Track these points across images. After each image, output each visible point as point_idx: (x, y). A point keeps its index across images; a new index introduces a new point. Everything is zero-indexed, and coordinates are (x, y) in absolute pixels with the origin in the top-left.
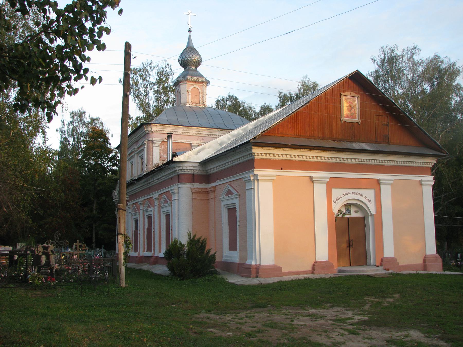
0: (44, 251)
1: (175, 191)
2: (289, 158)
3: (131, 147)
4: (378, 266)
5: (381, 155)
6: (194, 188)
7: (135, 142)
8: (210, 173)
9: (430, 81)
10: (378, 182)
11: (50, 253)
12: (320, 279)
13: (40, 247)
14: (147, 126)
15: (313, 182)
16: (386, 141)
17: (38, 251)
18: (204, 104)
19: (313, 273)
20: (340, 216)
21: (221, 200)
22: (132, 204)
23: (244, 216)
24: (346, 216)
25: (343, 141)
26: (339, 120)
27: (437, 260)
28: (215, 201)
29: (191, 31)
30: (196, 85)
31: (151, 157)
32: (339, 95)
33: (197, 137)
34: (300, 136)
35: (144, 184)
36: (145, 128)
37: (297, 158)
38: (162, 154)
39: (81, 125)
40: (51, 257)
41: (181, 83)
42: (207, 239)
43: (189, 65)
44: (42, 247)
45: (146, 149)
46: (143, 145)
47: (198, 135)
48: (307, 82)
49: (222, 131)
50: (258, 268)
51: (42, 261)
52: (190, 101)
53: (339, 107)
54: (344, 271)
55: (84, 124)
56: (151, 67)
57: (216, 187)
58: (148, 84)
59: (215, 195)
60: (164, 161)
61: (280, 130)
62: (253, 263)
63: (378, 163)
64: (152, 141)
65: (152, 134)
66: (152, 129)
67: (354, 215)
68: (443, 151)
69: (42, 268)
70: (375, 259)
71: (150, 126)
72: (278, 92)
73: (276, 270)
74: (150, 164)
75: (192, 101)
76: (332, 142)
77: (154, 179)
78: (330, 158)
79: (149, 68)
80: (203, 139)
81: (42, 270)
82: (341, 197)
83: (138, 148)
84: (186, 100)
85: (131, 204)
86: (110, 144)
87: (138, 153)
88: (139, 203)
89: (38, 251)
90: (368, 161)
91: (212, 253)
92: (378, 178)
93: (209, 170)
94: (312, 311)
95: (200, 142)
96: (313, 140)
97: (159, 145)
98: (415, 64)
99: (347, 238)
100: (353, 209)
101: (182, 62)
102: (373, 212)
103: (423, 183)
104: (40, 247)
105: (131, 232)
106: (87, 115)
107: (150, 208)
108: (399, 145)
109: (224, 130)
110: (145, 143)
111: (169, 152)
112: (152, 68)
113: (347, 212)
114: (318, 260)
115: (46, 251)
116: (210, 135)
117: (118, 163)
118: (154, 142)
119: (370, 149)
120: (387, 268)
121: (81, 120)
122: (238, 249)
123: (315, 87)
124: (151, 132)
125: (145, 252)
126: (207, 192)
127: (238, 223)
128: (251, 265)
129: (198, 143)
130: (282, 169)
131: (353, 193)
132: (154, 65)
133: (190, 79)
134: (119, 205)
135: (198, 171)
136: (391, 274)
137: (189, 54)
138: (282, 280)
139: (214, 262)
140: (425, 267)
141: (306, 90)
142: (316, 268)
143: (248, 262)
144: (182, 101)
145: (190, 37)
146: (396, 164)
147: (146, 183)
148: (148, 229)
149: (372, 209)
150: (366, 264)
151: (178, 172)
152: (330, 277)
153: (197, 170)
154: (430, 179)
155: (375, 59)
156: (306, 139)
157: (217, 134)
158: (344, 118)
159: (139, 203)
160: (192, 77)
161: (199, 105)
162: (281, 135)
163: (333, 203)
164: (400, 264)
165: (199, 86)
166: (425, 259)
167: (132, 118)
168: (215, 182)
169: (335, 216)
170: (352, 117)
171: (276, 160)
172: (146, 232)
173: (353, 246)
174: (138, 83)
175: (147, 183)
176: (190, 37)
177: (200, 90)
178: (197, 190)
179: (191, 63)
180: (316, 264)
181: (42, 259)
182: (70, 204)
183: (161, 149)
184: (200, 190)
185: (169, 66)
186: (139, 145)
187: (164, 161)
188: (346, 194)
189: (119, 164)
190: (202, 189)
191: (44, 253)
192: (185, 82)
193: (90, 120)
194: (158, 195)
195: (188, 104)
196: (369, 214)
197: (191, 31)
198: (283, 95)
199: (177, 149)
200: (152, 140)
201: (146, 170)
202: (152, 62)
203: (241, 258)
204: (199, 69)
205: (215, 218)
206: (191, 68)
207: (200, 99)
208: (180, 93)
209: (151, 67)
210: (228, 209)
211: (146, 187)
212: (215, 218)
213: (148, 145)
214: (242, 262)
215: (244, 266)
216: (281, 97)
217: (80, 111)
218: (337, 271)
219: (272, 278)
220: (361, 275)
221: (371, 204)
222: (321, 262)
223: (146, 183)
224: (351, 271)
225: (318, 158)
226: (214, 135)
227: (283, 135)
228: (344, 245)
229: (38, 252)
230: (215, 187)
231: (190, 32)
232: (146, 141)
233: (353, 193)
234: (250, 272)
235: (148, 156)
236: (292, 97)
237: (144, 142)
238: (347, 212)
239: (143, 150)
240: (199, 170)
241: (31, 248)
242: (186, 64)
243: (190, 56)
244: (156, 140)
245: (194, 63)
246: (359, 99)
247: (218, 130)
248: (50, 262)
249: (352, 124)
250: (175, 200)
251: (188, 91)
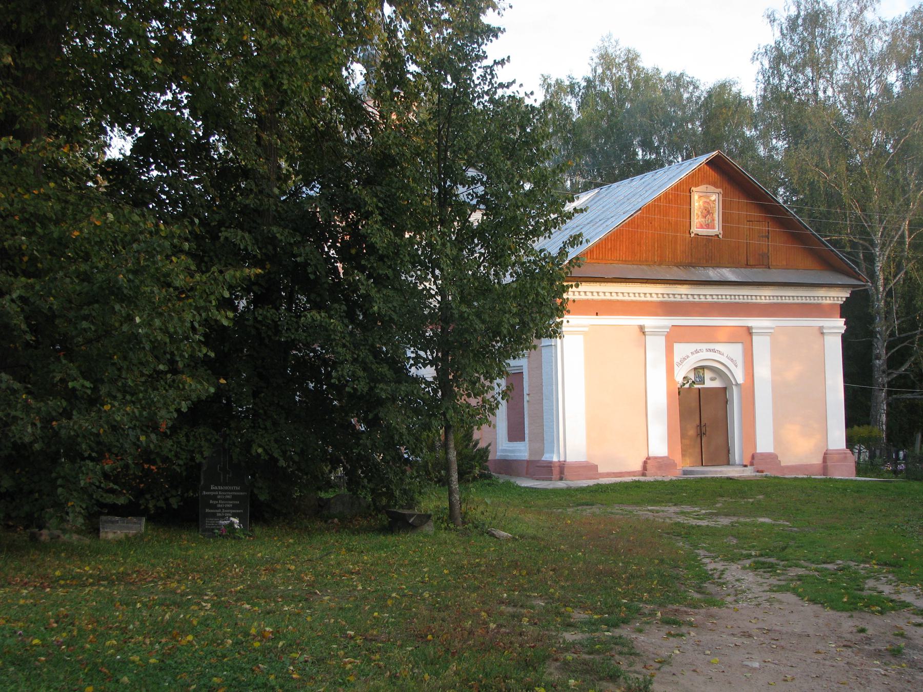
2: (608, 297)
4: (745, 466)
5: (755, 287)
9: (903, 63)
10: (749, 331)
12: (656, 481)
15: (644, 333)
16: (763, 262)
19: (644, 475)
20: (687, 386)
23: (538, 388)
24: (696, 386)
25: (693, 267)
26: (687, 232)
27: (845, 458)
32: (688, 191)
34: (626, 261)
37: (620, 297)
41: (576, 293)
48: (610, 51)
50: (562, 466)
53: (688, 212)
54: (691, 472)
61: (595, 252)
62: (555, 459)
63: (749, 301)
67: (709, 384)
68: (860, 277)
70: (741, 456)
73: (589, 468)
76: (675, 268)
78: (671, 296)
82: (688, 357)
90: (733, 297)
91: (482, 445)
92: (750, 325)
94: (650, 508)
96: (645, 267)
98: (870, 31)
99: (698, 422)
100: (708, 375)
102: (740, 380)
103: (825, 331)
108: (786, 268)
113: (698, 380)
114: (651, 455)
119: (736, 280)
120: (760, 469)
122: (527, 439)
123: (633, 60)
127: (526, 398)
128: (551, 462)
130: (597, 314)
131: (707, 350)
136: (766, 476)
138: (600, 483)
139: (487, 461)
140: (825, 467)
141: (609, 69)
142: (648, 466)
143: (546, 457)
146: (780, 301)
149: (739, 376)
150: (728, 464)
152: (671, 480)
154: (839, 324)
155: (777, 16)
156: (635, 267)
158: (695, 229)
162: (596, 261)
163: (675, 366)
164: (783, 464)
166: (826, 456)
169: (679, 386)
170: (708, 226)
171: (587, 301)
173: (707, 433)
180: (648, 461)
188: (697, 352)
196: (734, 383)
198: (553, 82)
203: (531, 452)
214: (533, 458)
215: (538, 464)
216: (549, 85)
218: (681, 472)
219: (584, 481)
220: (717, 478)
221: (736, 366)
222: (655, 458)
224: (702, 472)
225: (653, 295)
227: (599, 261)
228: (692, 432)
233: (707, 350)
234: (551, 472)
236: (576, 86)
238: (698, 380)
246: (721, 196)
249: (708, 238)
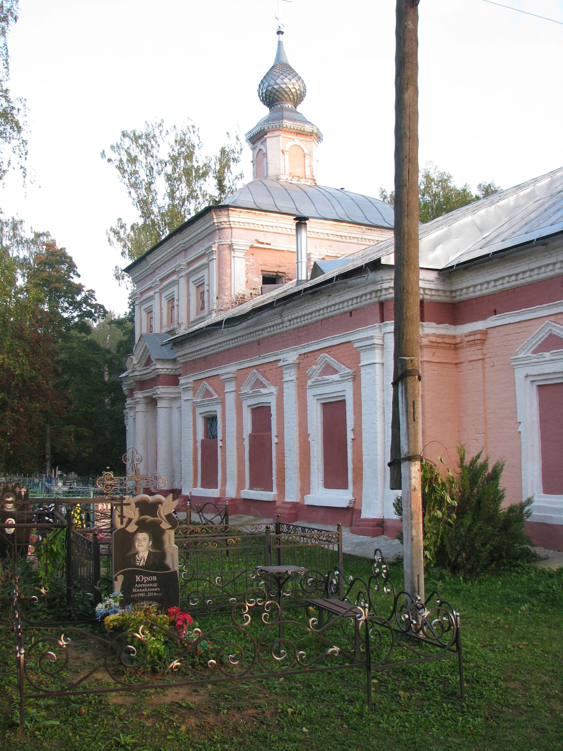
0: (145, 520)
1: (376, 341)
3: (169, 263)
6: (427, 335)
7: (180, 252)
8: (464, 297)
11: (165, 525)
13: (129, 504)
14: (219, 213)
17: (122, 517)
18: (314, 180)
21: (513, 364)
22: (194, 381)
28: (484, 368)
29: (282, 33)
30: (297, 140)
31: (227, 279)
33: (319, 241)
35: (244, 332)
36: (214, 217)
38: (250, 275)
39: (16, 245)
40: (166, 537)
41: (269, 135)
42: (504, 465)
43: (281, 99)
44: (138, 504)
45: (214, 265)
46: (207, 254)
47: (321, 236)
49: (370, 231)
51: (137, 553)
52: (287, 172)
55: (21, 242)
56: (161, 132)
57: (489, 331)
58: (156, 163)
59: (485, 351)
60: (254, 289)
64: (231, 246)
65: (230, 230)
66: (231, 219)
69: (138, 578)
71: (226, 213)
72: (379, 189)
74: (226, 296)
75: (292, 171)
77: (286, 319)
79: (157, 133)
80: (331, 246)
81: (139, 583)
83: (189, 264)
84: (280, 169)
85: (191, 380)
86: (79, 276)
87: (188, 276)
88: (222, 378)
89: (122, 517)
93: (455, 291)
95: (326, 251)
97: (244, 254)
101: (268, 93)
104: (129, 504)
105: (192, 442)
106: (25, 226)
107: (264, 386)
109: (372, 228)
110: (213, 249)
111: (300, 260)
112: (164, 133)
115: (149, 518)
116: (346, 237)
117: (93, 311)
118: (235, 247)
121: (15, 236)
123: (446, 180)
124: (226, 226)
125: (246, 490)
126: (452, 346)
129: (322, 253)
130: (495, 313)
132: (167, 126)
133: (289, 127)
134: (412, 361)
135: (433, 293)
137: (282, 77)
144: (271, 172)
145: (280, 43)
147: (252, 330)
148: (253, 438)
151: (384, 292)
153: (431, 290)
157: (360, 236)
159: (222, 378)
160: (292, 123)
161: (304, 180)
165: (304, 142)
167: (126, 224)
168: (484, 318)
172: (246, 443)
174: (137, 160)
175: (258, 328)
176: (280, 43)
177: (306, 151)
178: (433, 339)
179: (286, 96)
181: (137, 544)
182: (39, 383)
183: (247, 263)
184: (440, 340)
185: (196, 130)
186: (190, 257)
187: (254, 289)
189: (95, 312)
190: (443, 336)
191: (142, 526)
192: (276, 133)
193: (32, 236)
194: (296, 357)
195: (283, 178)
197: (282, 33)
199: (280, 264)
200: (230, 243)
201: (215, 308)
202: (163, 121)
204: (299, 108)
205: (485, 411)
206: (287, 106)
207: (308, 169)
208: (265, 155)
209: (161, 132)
210: (539, 386)
211: (251, 340)
212: (485, 411)
213: (219, 255)
217: (13, 218)
223: (252, 330)
226: (354, 238)
229: (125, 520)
230: (485, 332)
231: (280, 35)
232: (217, 245)
235: (220, 278)
237: (211, 247)
239: (206, 266)
240: (437, 290)
241: (18, 490)
242: (276, 97)
243: (284, 81)
244: (239, 243)
245: (291, 97)
247: (361, 227)
248: (163, 556)
250: (375, 363)
251: (283, 152)
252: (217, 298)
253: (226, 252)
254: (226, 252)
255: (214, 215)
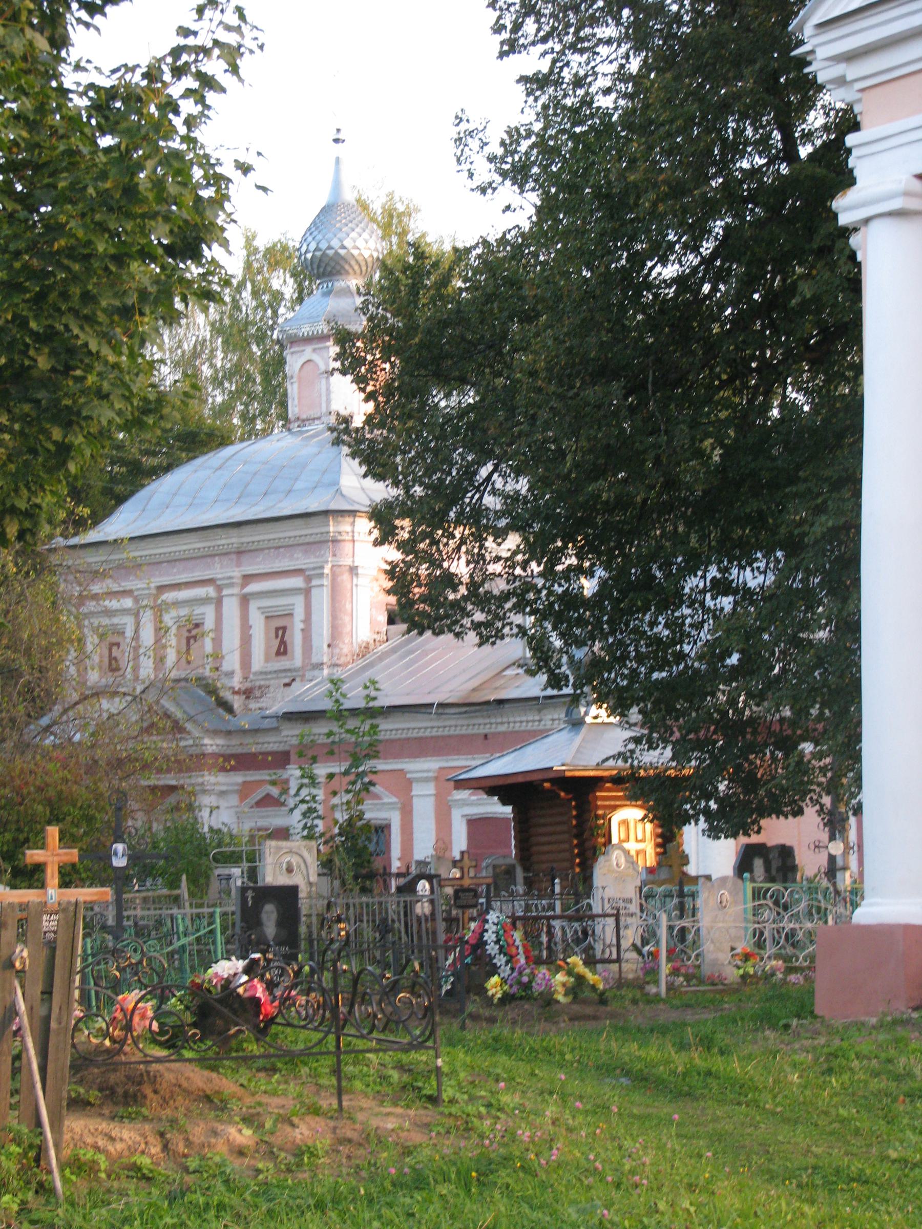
14: (340, 519)
31: (347, 619)
211: (470, 731)
232: (330, 565)
252: (329, 646)
253: (346, 577)
254: (346, 577)
255: (331, 523)
